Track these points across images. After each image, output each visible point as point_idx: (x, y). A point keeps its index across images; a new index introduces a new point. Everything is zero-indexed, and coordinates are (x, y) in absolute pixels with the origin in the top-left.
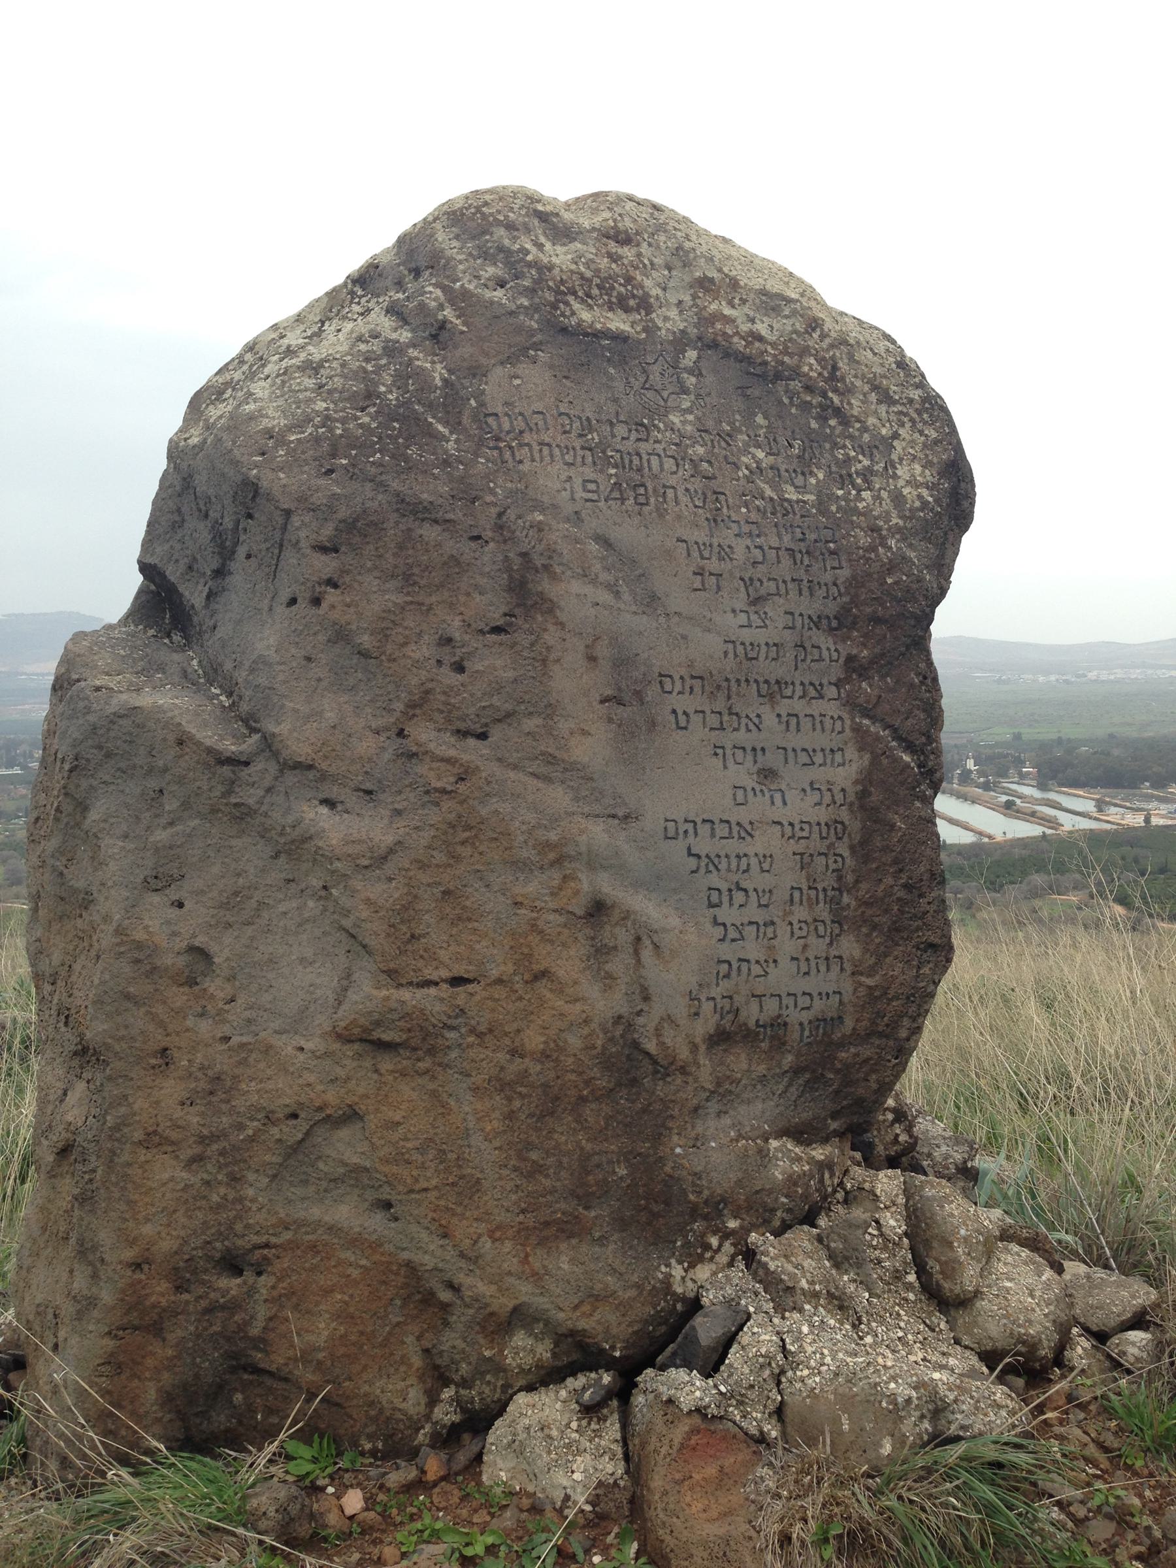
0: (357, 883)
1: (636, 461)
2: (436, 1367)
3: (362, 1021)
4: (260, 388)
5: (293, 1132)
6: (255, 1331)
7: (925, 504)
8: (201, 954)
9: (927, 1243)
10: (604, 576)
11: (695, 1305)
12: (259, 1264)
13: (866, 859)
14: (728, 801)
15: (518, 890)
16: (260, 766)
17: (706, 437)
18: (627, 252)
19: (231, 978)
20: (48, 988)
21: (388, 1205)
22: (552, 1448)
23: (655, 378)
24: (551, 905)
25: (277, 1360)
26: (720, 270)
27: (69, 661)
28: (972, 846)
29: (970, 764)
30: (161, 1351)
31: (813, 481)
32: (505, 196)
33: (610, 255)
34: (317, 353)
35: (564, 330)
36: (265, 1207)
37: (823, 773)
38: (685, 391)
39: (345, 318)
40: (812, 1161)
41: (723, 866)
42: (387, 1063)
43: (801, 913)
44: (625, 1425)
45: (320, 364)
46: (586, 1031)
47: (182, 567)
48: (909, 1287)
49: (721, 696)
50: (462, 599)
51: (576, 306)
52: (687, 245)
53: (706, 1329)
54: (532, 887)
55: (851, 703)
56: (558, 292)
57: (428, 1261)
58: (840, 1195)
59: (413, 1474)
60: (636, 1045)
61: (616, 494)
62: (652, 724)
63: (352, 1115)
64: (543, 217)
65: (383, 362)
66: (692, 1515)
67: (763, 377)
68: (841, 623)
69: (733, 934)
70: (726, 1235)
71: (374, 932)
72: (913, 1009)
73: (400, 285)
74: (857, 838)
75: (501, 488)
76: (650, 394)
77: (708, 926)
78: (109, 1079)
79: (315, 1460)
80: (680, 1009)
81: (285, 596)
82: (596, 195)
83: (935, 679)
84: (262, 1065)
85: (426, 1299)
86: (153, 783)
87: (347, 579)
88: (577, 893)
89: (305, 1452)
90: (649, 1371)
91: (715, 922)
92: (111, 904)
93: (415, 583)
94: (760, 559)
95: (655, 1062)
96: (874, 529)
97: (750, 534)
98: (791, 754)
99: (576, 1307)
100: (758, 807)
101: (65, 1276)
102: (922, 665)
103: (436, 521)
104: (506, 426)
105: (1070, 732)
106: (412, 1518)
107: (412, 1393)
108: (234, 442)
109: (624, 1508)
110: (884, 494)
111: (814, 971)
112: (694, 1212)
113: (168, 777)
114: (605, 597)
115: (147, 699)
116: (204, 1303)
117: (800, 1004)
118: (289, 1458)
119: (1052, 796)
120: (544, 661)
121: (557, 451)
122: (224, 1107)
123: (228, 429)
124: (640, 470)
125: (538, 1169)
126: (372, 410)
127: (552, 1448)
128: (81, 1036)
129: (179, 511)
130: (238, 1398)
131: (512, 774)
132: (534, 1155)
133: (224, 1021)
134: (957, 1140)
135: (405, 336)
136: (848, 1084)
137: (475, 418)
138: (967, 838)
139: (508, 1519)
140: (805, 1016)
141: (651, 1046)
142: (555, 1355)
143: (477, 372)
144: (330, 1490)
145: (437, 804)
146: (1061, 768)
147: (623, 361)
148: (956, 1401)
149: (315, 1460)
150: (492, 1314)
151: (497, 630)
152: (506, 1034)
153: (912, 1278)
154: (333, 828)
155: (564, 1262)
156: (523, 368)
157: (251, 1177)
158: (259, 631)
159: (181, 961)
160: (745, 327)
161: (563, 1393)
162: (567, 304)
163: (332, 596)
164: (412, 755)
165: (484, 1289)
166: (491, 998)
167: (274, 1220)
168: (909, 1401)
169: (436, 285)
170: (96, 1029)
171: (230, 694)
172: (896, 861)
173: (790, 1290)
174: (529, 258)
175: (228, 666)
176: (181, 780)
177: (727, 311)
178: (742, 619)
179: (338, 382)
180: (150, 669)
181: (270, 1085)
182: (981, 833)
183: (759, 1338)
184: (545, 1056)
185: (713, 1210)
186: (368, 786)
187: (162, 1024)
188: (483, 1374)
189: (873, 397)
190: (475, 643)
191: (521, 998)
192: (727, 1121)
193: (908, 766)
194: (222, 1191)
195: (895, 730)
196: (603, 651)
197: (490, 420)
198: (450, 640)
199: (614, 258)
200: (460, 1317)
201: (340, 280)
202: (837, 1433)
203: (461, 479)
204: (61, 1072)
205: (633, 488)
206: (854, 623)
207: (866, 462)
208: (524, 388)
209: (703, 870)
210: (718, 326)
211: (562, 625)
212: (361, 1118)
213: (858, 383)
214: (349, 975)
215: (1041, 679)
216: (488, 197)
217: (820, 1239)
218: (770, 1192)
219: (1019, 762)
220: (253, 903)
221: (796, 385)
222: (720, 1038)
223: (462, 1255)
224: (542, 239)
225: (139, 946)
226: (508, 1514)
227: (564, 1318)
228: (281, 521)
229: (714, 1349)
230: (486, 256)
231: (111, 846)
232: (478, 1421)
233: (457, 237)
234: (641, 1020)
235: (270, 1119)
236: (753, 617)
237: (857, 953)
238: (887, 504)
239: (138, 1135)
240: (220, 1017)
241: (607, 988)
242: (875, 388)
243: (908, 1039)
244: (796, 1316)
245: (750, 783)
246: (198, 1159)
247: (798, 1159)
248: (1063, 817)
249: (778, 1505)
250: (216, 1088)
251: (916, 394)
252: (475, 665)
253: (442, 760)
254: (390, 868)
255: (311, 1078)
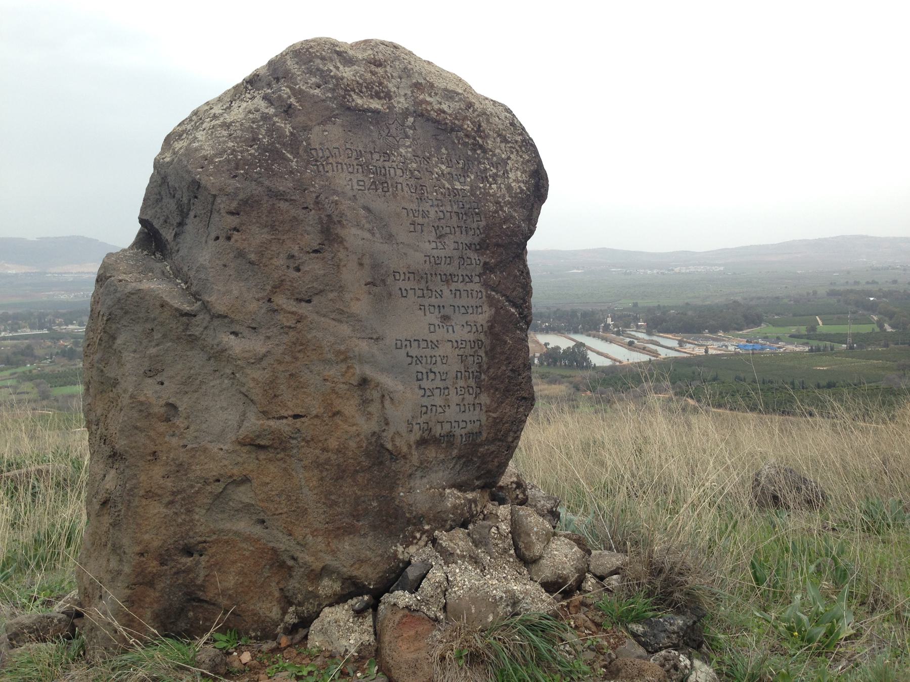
0: (248, 371)
1: (383, 171)
2: (286, 597)
3: (251, 436)
4: (200, 135)
5: (218, 488)
6: (199, 582)
7: (522, 190)
8: (172, 406)
9: (520, 536)
10: (367, 226)
11: (409, 563)
12: (201, 551)
13: (493, 358)
14: (426, 331)
15: (326, 373)
16: (201, 317)
17: (417, 159)
18: (380, 71)
19: (187, 418)
20: (94, 427)
21: (263, 522)
22: (340, 630)
23: (393, 131)
24: (342, 380)
25: (210, 595)
26: (425, 79)
27: (105, 267)
28: (611, 367)
29: (609, 321)
30: (153, 594)
31: (469, 180)
32: (321, 43)
33: (371, 72)
34: (229, 118)
35: (349, 108)
36: (204, 523)
37: (471, 318)
38: (407, 137)
39: (242, 100)
40: (465, 498)
41: (424, 361)
42: (262, 456)
43: (461, 383)
44: (374, 621)
45: (231, 124)
46: (358, 439)
47: (161, 221)
48: (511, 556)
49: (423, 282)
50: (299, 237)
51: (355, 97)
52: (409, 67)
53: (412, 573)
54: (332, 372)
55: (486, 285)
56: (346, 90)
57: (282, 547)
58: (481, 517)
59: (274, 644)
60: (382, 446)
61: (373, 187)
62: (390, 295)
63: (245, 480)
64: (339, 54)
65: (261, 123)
66: (401, 652)
67: (445, 130)
68: (481, 247)
69: (428, 393)
70: (424, 532)
71: (256, 393)
72: (515, 428)
73: (269, 85)
74: (488, 348)
75: (318, 184)
76: (390, 139)
77: (417, 390)
78: (127, 467)
79: (228, 641)
80: (403, 429)
81: (213, 235)
82: (366, 41)
83: (528, 273)
84: (202, 457)
85: (281, 565)
86: (149, 326)
87: (244, 228)
88: (354, 374)
89: (224, 638)
90: (387, 594)
91: (420, 388)
92: (128, 384)
93: (276, 229)
94: (442, 216)
95: (391, 454)
96: (498, 203)
97: (438, 205)
98: (457, 309)
99: (352, 566)
100: (441, 333)
101: (105, 563)
102: (521, 267)
103: (286, 200)
104: (321, 155)
105: (664, 302)
106: (274, 663)
107: (275, 609)
108: (188, 162)
109: (373, 654)
110: (502, 186)
111: (467, 410)
112: (409, 522)
113: (156, 322)
114: (367, 235)
115: (145, 285)
116: (174, 570)
117: (461, 426)
118: (215, 641)
119: (655, 338)
120: (338, 266)
121: (345, 167)
122: (184, 478)
123: (185, 155)
124: (385, 175)
125: (335, 503)
126: (256, 147)
127: (340, 630)
128: (113, 447)
129: (160, 193)
130: (191, 614)
131: (323, 319)
132: (333, 497)
133: (184, 438)
134: (549, 498)
135: (272, 111)
136: (484, 463)
137: (306, 151)
138: (607, 363)
139: (319, 662)
140: (463, 432)
141: (389, 446)
142: (342, 589)
143: (306, 129)
144: (235, 654)
145: (287, 333)
146: (660, 322)
147: (378, 123)
148: (523, 598)
149: (228, 641)
150: (312, 570)
151: (316, 251)
152: (320, 441)
153: (512, 552)
154: (236, 345)
155: (346, 545)
156: (329, 127)
157: (197, 510)
158: (201, 252)
159: (163, 410)
160: (436, 107)
161: (346, 607)
162: (350, 96)
163: (236, 236)
164: (275, 311)
165: (309, 559)
166: (313, 424)
167: (208, 530)
168: (501, 598)
169: (287, 87)
170: (121, 444)
171: (186, 283)
172: (507, 359)
173: (452, 554)
174: (332, 74)
175: (185, 269)
176: (162, 324)
177: (428, 99)
178: (434, 245)
179: (239, 133)
180: (146, 271)
181: (206, 466)
182: (615, 360)
183: (437, 575)
184: (338, 451)
185: (417, 521)
186: (254, 325)
187: (153, 440)
188: (308, 599)
189: (498, 140)
190: (305, 257)
191: (327, 425)
192: (425, 480)
193: (513, 314)
194: (183, 517)
195: (507, 297)
196: (366, 261)
197: (313, 152)
198: (293, 256)
199: (373, 73)
200: (298, 573)
201: (240, 81)
202: (469, 614)
203: (298, 180)
204: (102, 466)
205: (382, 184)
206: (488, 247)
207: (494, 171)
208: (329, 136)
209: (414, 363)
210: (424, 106)
211: (347, 249)
212: (250, 481)
213: (491, 133)
214: (244, 415)
215: (649, 272)
216: (312, 44)
217: (469, 534)
218: (445, 512)
219: (636, 319)
220: (198, 382)
221: (461, 134)
222: (422, 442)
223: (298, 543)
224: (339, 64)
225: (142, 403)
226: (319, 659)
227: (346, 571)
228: (211, 200)
229: (416, 581)
230: (310, 72)
231: (128, 356)
232: (305, 622)
233: (297, 63)
234: (385, 434)
235: (206, 482)
236: (439, 244)
237: (488, 402)
238: (504, 191)
239: (142, 493)
240: (182, 436)
241: (369, 419)
242: (499, 135)
243: (512, 442)
244: (454, 565)
245: (437, 322)
246: (171, 503)
247: (459, 498)
248: (659, 349)
249: (441, 646)
250: (180, 469)
251: (519, 138)
252: (305, 268)
253: (289, 313)
254: (264, 363)
255: (226, 463)
